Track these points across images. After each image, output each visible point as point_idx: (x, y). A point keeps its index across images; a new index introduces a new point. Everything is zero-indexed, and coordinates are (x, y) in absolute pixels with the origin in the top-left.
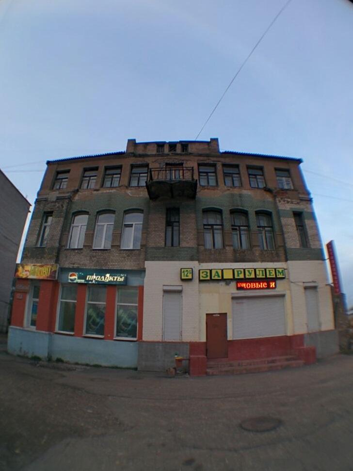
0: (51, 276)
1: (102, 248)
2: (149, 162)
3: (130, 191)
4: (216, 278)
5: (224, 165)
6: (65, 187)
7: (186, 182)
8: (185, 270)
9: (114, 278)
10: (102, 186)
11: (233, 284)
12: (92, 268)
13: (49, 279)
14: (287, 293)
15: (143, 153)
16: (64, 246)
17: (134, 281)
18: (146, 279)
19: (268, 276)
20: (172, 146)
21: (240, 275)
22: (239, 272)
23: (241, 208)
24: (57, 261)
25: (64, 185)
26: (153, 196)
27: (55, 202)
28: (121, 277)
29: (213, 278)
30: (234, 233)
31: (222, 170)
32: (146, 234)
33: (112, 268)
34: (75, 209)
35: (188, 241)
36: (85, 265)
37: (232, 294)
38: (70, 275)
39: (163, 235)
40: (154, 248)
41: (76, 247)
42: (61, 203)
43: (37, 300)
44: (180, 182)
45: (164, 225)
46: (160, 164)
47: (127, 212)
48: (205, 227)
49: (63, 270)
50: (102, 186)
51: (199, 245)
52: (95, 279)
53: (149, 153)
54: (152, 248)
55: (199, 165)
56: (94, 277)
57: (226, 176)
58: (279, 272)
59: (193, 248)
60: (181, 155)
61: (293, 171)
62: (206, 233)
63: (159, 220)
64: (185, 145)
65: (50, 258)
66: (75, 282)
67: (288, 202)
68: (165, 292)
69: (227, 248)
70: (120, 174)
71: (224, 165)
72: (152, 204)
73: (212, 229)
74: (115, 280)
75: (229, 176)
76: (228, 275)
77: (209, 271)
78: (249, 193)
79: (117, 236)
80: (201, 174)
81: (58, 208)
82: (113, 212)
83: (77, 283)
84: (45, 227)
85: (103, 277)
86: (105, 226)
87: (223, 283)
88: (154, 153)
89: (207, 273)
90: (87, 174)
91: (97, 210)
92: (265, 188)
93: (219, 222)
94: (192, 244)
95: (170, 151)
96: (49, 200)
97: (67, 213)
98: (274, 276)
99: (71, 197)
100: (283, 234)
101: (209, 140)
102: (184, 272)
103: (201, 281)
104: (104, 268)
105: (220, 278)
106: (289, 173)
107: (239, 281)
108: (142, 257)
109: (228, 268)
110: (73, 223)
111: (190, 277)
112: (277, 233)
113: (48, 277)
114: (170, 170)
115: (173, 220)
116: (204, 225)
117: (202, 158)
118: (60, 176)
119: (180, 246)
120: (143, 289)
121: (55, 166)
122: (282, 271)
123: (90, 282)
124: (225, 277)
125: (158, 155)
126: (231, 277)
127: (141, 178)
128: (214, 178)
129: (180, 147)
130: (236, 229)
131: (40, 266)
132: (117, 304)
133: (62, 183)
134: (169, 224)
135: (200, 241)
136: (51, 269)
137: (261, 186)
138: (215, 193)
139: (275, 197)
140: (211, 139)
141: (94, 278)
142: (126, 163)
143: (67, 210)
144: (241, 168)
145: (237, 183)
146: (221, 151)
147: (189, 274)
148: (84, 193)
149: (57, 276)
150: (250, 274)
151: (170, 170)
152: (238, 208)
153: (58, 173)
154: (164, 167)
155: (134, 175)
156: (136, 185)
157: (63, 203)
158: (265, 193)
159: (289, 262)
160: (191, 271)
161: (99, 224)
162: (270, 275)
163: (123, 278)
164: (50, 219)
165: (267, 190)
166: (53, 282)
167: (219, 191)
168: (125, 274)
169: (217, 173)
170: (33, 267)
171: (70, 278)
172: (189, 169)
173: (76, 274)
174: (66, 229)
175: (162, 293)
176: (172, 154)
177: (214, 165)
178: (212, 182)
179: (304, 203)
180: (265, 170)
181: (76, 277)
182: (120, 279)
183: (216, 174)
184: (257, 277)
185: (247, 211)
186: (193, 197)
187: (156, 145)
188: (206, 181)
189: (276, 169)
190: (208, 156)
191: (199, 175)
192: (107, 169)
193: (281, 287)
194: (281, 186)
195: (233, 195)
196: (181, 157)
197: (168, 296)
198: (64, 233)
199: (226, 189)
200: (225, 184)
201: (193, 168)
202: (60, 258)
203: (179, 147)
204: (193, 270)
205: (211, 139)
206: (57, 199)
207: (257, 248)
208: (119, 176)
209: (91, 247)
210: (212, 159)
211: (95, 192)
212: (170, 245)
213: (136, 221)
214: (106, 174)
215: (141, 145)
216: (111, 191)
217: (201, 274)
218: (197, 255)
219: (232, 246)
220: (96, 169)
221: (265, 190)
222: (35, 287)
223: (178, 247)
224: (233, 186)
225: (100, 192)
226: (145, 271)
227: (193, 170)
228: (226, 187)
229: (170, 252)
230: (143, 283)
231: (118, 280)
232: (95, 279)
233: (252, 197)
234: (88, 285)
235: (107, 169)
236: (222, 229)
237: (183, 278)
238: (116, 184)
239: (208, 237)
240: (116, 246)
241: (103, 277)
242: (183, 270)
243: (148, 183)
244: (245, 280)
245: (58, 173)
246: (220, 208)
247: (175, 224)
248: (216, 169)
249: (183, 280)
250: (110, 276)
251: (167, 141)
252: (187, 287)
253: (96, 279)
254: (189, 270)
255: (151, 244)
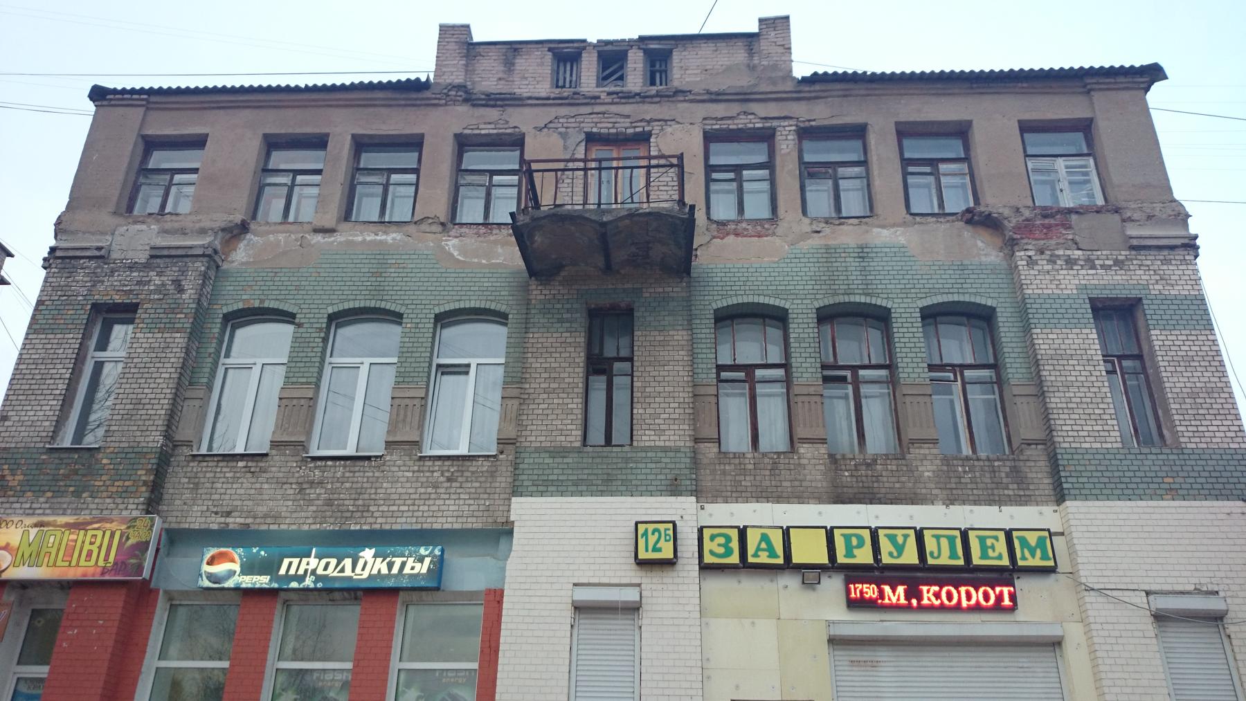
0: (119, 565)
1: (350, 451)
2: (523, 129)
3: (455, 241)
4: (764, 558)
5: (807, 133)
6: (185, 207)
7: (656, 215)
8: (651, 527)
9: (390, 565)
10: (347, 216)
11: (833, 585)
12: (306, 527)
13: (107, 577)
14: (1074, 634)
15: (502, 88)
16: (188, 444)
17: (469, 573)
18: (512, 565)
19: (976, 561)
20: (612, 57)
21: (856, 552)
22: (854, 541)
23: (863, 299)
24: (153, 505)
25: (183, 202)
26: (539, 267)
27: (147, 266)
28: (421, 560)
29: (751, 560)
30: (833, 391)
31: (795, 154)
32: (516, 402)
33: (387, 527)
34: (233, 299)
35: (662, 425)
36: (277, 517)
37: (830, 623)
38: (207, 556)
39: (576, 404)
40: (546, 450)
41: (240, 450)
42: (172, 273)
43: (42, 671)
44: (632, 215)
45: (580, 370)
46: (564, 136)
47: (444, 319)
48: (724, 375)
49: (176, 538)
50: (347, 216)
51: (697, 440)
52: (314, 572)
53: (523, 90)
54: (538, 450)
55: (710, 138)
56: (313, 562)
57: (812, 176)
58: (1024, 542)
59: (677, 450)
60: (642, 98)
61: (1105, 128)
62: (727, 395)
63: (562, 354)
64: (659, 52)
65: (125, 493)
66: (230, 584)
67: (1070, 262)
68: (580, 609)
69: (803, 449)
70: (416, 171)
71: (807, 133)
72: (538, 293)
73: (751, 381)
74: (395, 570)
75: (824, 176)
76: (810, 550)
77: (734, 534)
78: (902, 240)
79: (412, 402)
80: (715, 176)
81: (158, 291)
82: (396, 317)
83: (237, 589)
84: (99, 366)
85: (348, 562)
86: (364, 370)
87: (791, 582)
88: (544, 88)
89: (728, 539)
90: (280, 159)
91: (330, 310)
92: (968, 211)
93: (775, 356)
94: (676, 436)
95: (603, 79)
96: (114, 255)
97: (200, 315)
98: (1005, 562)
99: (216, 252)
100: (1041, 393)
101: (754, 28)
102: (645, 533)
103: (705, 568)
104: (352, 528)
105: (781, 561)
106: (1090, 141)
107: (854, 573)
108: (503, 480)
109: (809, 522)
110: (227, 356)
111: (667, 553)
112: (1016, 391)
113: (104, 571)
114: (600, 169)
115: (609, 352)
116: (720, 368)
117: (719, 110)
118: (159, 159)
119: (635, 444)
120: (500, 602)
121: (135, 114)
122: (1041, 541)
123: (294, 585)
124: (796, 559)
125: (560, 101)
126: (824, 559)
127: (496, 192)
128: (765, 186)
129: (640, 66)
130: (843, 379)
131: (68, 526)
132: (395, 664)
133: (174, 190)
134: (597, 365)
135: (705, 431)
136: (125, 537)
137: (956, 202)
138: (762, 249)
139: (1011, 245)
140: (762, 21)
141: (311, 567)
142: (440, 127)
143: (199, 302)
144: (872, 139)
145: (853, 203)
146: (801, 70)
147: (662, 544)
148: (271, 238)
149: (147, 565)
150: (900, 549)
151: (600, 169)
152: (853, 299)
153: (151, 144)
154: (580, 153)
155: (470, 178)
156: (481, 221)
157: (183, 272)
158: (967, 232)
159: (1068, 503)
160: (671, 532)
161: (333, 360)
162: (984, 555)
163: (427, 560)
164: (120, 332)
165: (980, 219)
166: (130, 594)
167: (777, 241)
168: (435, 546)
169: (778, 169)
170: (33, 532)
171: (206, 568)
172: (662, 162)
173: (237, 553)
174: (195, 378)
175: (568, 613)
176: (609, 94)
177: (766, 137)
178: (757, 207)
179: (1148, 259)
180: (978, 135)
181: (236, 567)
182: (414, 565)
183: (773, 173)
184: (930, 561)
185: (888, 311)
186: (681, 265)
187: (549, 55)
188: (733, 199)
189: (1026, 128)
190: (744, 97)
191: (708, 180)
192: (361, 145)
193: (1037, 608)
194: (1043, 199)
195: (830, 252)
196: (646, 107)
197: (586, 622)
198: (188, 394)
199: (808, 229)
200: (804, 212)
201: (681, 157)
202: (169, 490)
203: (636, 63)
204: (679, 529)
205: (762, 21)
206: (152, 257)
207: (925, 450)
208: (412, 178)
209: (303, 446)
210: (761, 110)
211: (319, 238)
212: (601, 440)
213: (483, 350)
214: (358, 169)
215: (493, 53)
216: (381, 237)
217: (707, 545)
218: (690, 480)
219: (823, 441)
220: (319, 142)
221: (968, 222)
222: (35, 614)
223: (627, 448)
224: (838, 217)
225: (339, 238)
226: (510, 533)
227: (681, 166)
228: (806, 221)
229: (601, 460)
230: (504, 578)
231: (407, 570)
232: (314, 572)
233: (909, 250)
234: (282, 594)
235: (361, 145)
236: (788, 381)
237: (643, 555)
238: (401, 210)
239: (734, 408)
240: (405, 444)
241: (348, 562)
242: (641, 528)
243: (522, 219)
244: (879, 573)
245: (151, 144)
246: (781, 304)
247: (617, 366)
248: (772, 153)
249: (642, 564)
250: (375, 556)
251: (593, 39)
252: (656, 589)
253: (320, 571)
254: (661, 527)
255: (535, 437)
